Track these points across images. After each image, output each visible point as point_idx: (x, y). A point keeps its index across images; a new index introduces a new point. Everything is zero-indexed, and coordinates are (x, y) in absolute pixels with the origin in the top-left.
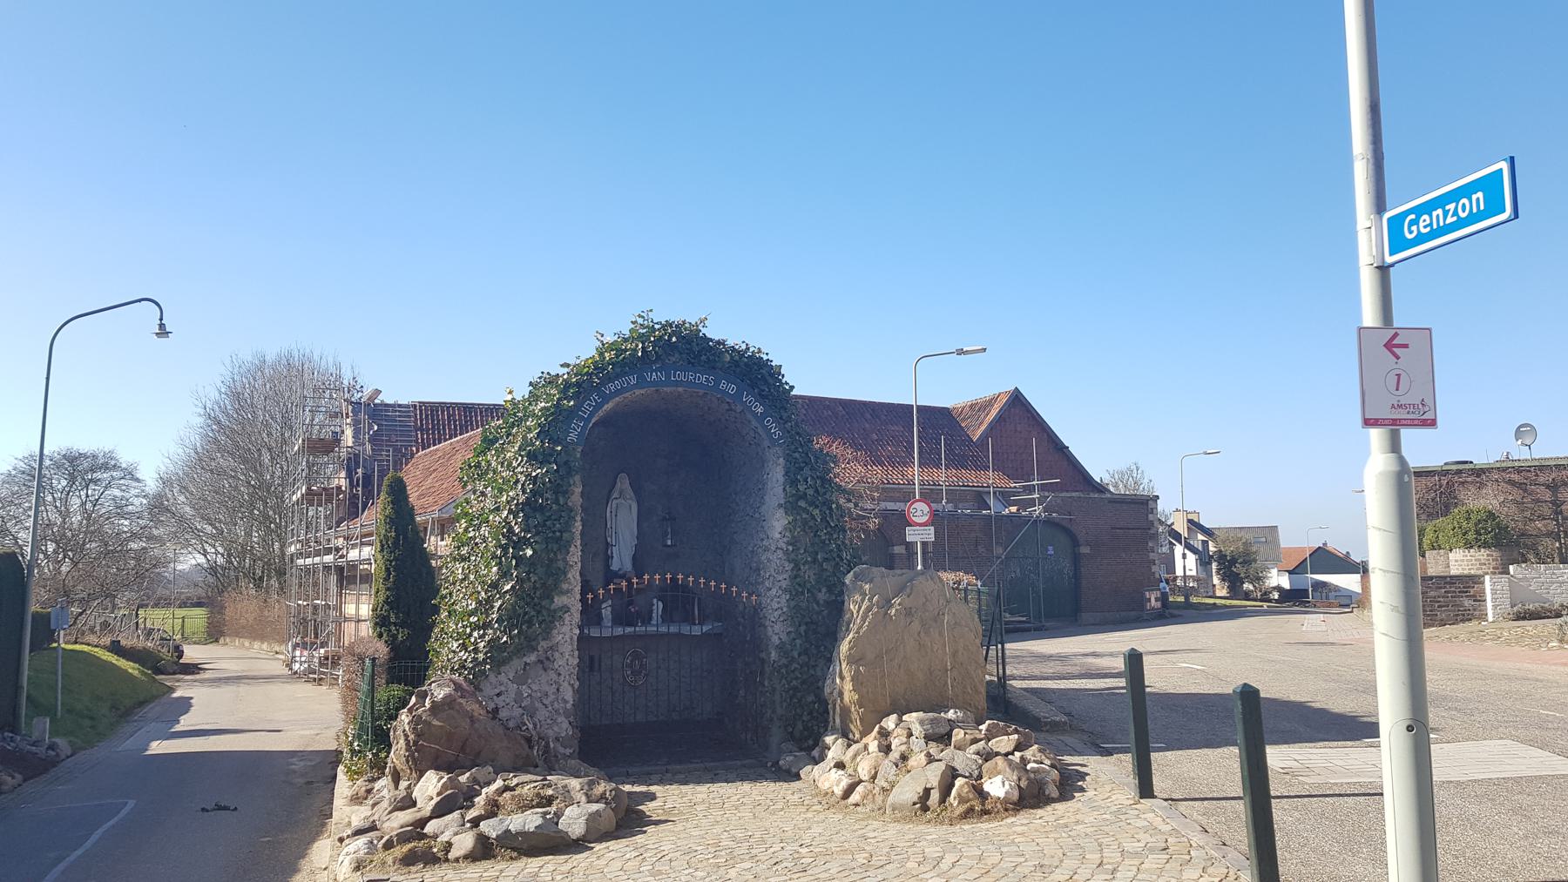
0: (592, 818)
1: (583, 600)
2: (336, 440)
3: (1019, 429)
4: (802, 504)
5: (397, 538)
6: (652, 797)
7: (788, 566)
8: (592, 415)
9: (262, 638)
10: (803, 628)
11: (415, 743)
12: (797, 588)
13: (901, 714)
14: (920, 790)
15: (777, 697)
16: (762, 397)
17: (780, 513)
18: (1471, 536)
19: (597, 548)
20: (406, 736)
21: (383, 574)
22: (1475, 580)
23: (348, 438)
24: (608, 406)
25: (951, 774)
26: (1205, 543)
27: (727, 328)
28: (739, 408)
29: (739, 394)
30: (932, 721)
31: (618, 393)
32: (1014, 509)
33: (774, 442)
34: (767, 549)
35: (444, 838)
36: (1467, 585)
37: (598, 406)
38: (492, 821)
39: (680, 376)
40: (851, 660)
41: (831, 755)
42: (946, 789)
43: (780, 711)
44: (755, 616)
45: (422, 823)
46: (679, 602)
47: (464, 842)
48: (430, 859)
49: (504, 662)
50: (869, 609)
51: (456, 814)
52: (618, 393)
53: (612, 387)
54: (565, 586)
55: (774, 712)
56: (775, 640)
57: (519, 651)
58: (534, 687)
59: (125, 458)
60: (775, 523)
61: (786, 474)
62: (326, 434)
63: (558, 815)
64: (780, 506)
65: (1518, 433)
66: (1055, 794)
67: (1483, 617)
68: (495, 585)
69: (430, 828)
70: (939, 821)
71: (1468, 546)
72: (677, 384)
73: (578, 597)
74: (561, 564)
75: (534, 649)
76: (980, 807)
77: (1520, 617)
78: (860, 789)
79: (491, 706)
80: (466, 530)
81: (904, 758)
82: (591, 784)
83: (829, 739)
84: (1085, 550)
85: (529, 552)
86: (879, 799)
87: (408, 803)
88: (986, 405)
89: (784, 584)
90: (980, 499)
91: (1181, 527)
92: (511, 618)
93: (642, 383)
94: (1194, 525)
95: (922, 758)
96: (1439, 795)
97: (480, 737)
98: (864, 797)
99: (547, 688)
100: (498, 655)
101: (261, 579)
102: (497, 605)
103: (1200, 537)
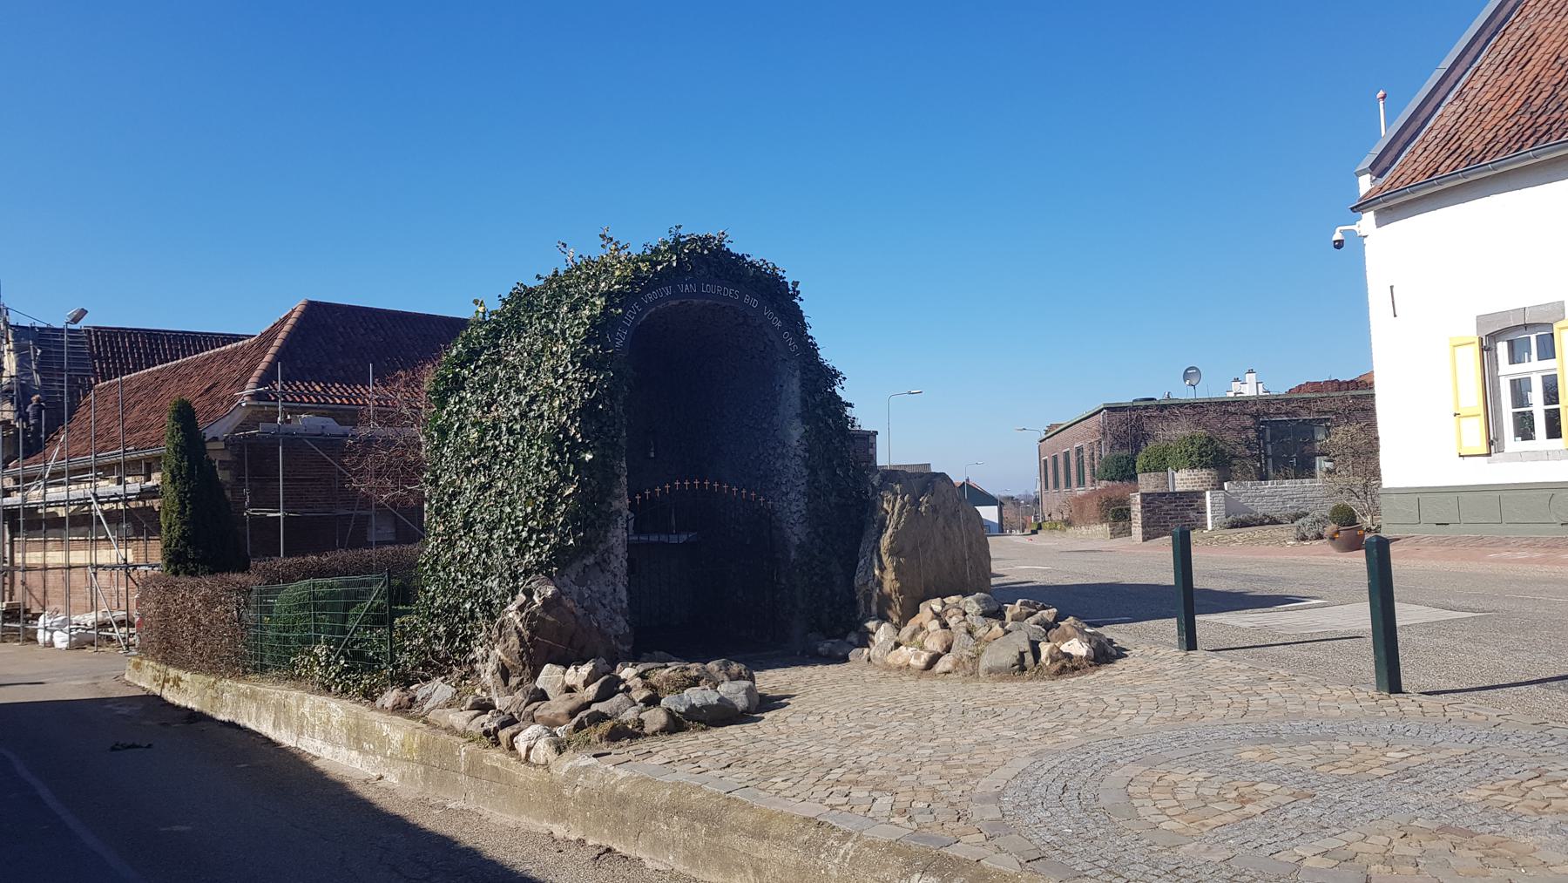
5: (191, 468)
10: (821, 529)
11: (530, 639)
17: (797, 423)
18: (1195, 458)
20: (519, 633)
22: (1199, 495)
27: (749, 244)
34: (783, 456)
36: (1192, 499)
39: (708, 288)
40: (893, 552)
47: (655, 718)
50: (903, 507)
53: (650, 297)
58: (594, 588)
61: (803, 385)
64: (798, 415)
65: (1186, 376)
67: (1204, 526)
68: (552, 490)
71: (1193, 467)
72: (706, 296)
77: (1233, 526)
82: (726, 664)
83: (871, 625)
85: (589, 457)
89: (802, 489)
96: (1401, 636)
99: (604, 589)
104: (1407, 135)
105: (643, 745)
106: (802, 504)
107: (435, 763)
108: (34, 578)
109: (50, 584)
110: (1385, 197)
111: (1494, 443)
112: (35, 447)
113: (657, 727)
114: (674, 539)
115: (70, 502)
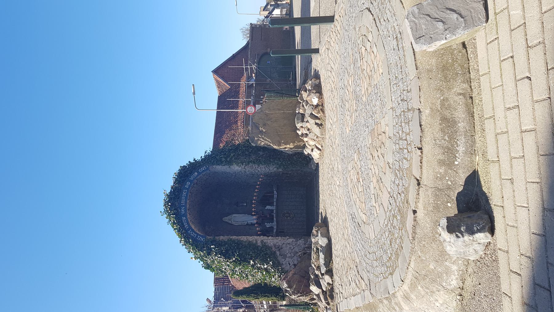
0: (322, 235)
1: (260, 235)
4: (228, 159)
5: (254, 293)
6: (321, 212)
7: (251, 164)
8: (195, 233)
10: (271, 160)
12: (258, 162)
13: (297, 129)
14: (316, 126)
15: (294, 169)
16: (191, 173)
19: (247, 229)
20: (299, 296)
21: (266, 298)
24: (193, 227)
25: (312, 116)
26: (271, 5)
27: (168, 184)
28: (196, 181)
29: (191, 181)
30: (298, 119)
31: (188, 224)
32: (253, 75)
33: (208, 169)
35: (326, 284)
37: (193, 230)
38: (321, 269)
39: (183, 202)
40: (279, 145)
41: (310, 152)
42: (317, 118)
43: (299, 168)
44: (266, 175)
45: (323, 291)
46: (266, 200)
47: (327, 278)
48: (332, 290)
49: (279, 262)
50: (263, 138)
51: (321, 280)
52: (188, 224)
53: (186, 226)
54: (254, 242)
55: (299, 170)
56: (275, 169)
57: (276, 258)
60: (236, 169)
63: (321, 247)
66: (318, 81)
69: (324, 289)
70: (324, 121)
72: (186, 203)
73: (258, 237)
74: (246, 244)
75: (275, 252)
76: (320, 107)
78: (317, 145)
79: (293, 267)
80: (237, 275)
81: (308, 130)
82: (313, 235)
86: (320, 139)
87: (318, 295)
88: (218, 83)
89: (257, 166)
91: (266, 13)
92: (264, 261)
93: (185, 215)
94: (265, 9)
95: (307, 124)
97: (300, 271)
98: (319, 144)
100: (277, 265)
102: (259, 266)
103: (269, 7)
105: (336, 284)
106: (262, 166)
113: (330, 279)
114: (275, 196)
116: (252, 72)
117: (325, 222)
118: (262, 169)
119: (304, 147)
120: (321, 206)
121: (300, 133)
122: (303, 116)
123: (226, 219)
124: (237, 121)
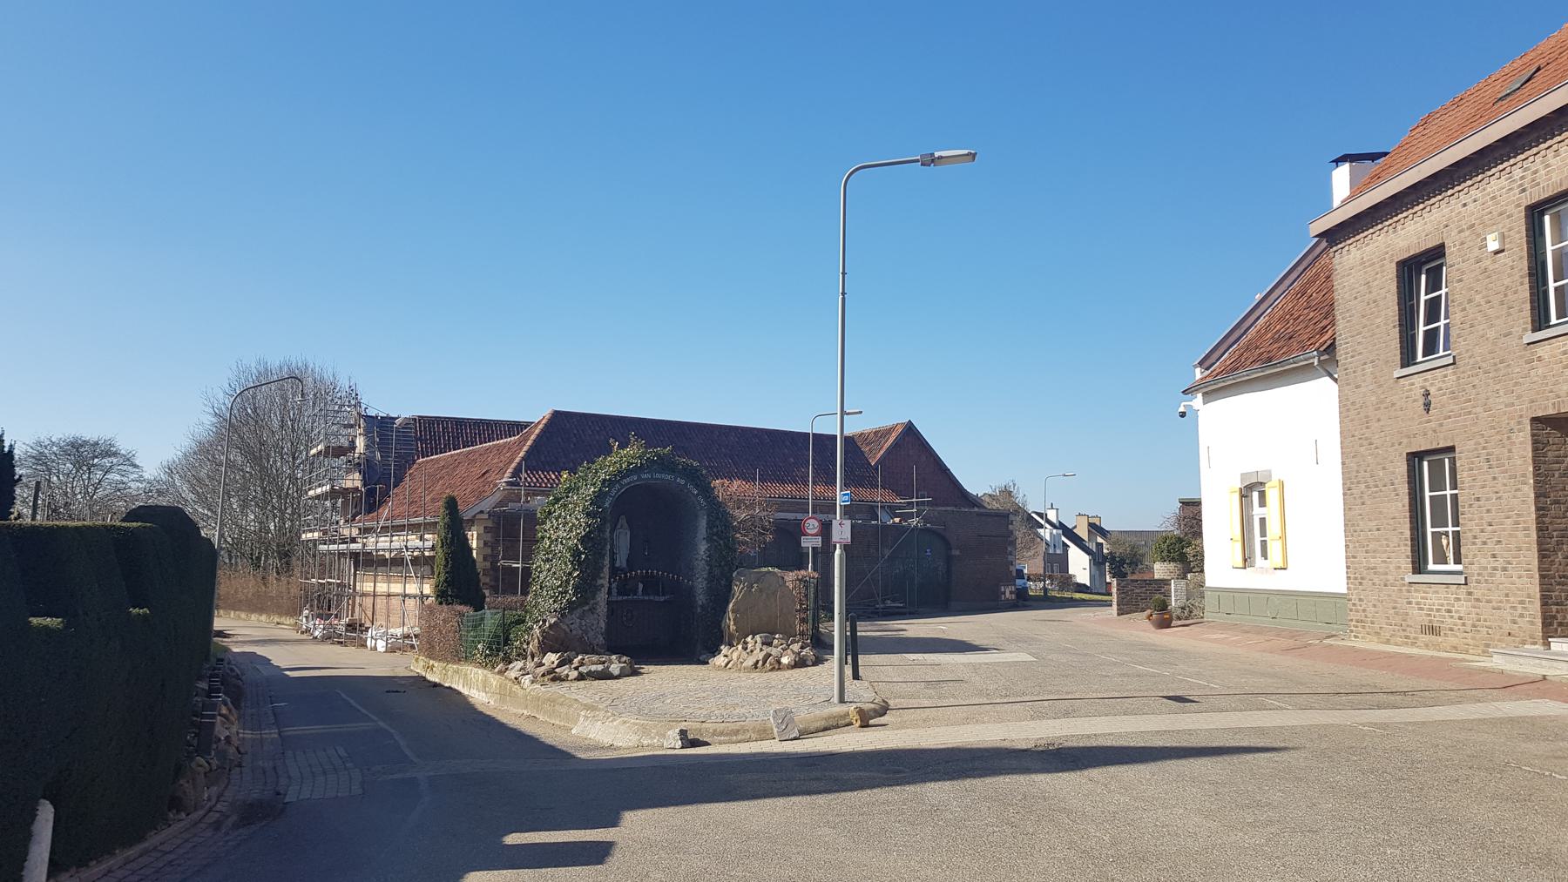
2: (353, 447)
3: (909, 458)
9: (261, 610)
12: (711, 578)
16: (697, 486)
22: (1166, 582)
23: (360, 443)
39: (658, 476)
44: (691, 591)
46: (651, 584)
59: (123, 446)
62: (344, 442)
76: (778, 666)
84: (956, 552)
90: (872, 512)
94: (1095, 529)
101: (259, 559)
104: (1231, 339)
105: (566, 684)
107: (503, 694)
108: (368, 601)
109: (378, 607)
110: (1207, 384)
111: (1247, 561)
112: (372, 507)
115: (391, 551)
116: (905, 517)
117: (635, 673)
118: (700, 584)
119: (731, 645)
120: (652, 668)
121: (749, 639)
122: (770, 644)
123: (623, 521)
124: (796, 482)
